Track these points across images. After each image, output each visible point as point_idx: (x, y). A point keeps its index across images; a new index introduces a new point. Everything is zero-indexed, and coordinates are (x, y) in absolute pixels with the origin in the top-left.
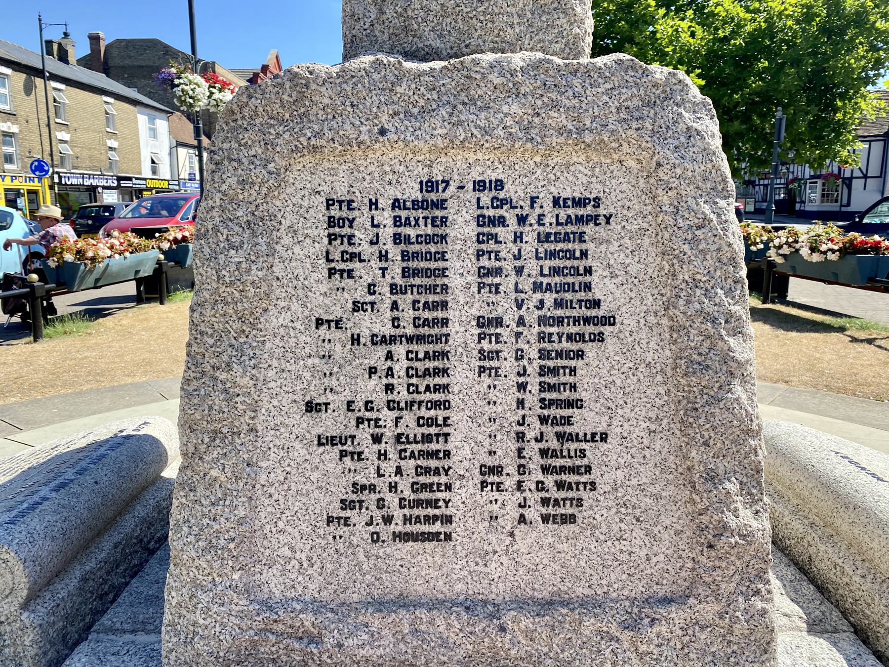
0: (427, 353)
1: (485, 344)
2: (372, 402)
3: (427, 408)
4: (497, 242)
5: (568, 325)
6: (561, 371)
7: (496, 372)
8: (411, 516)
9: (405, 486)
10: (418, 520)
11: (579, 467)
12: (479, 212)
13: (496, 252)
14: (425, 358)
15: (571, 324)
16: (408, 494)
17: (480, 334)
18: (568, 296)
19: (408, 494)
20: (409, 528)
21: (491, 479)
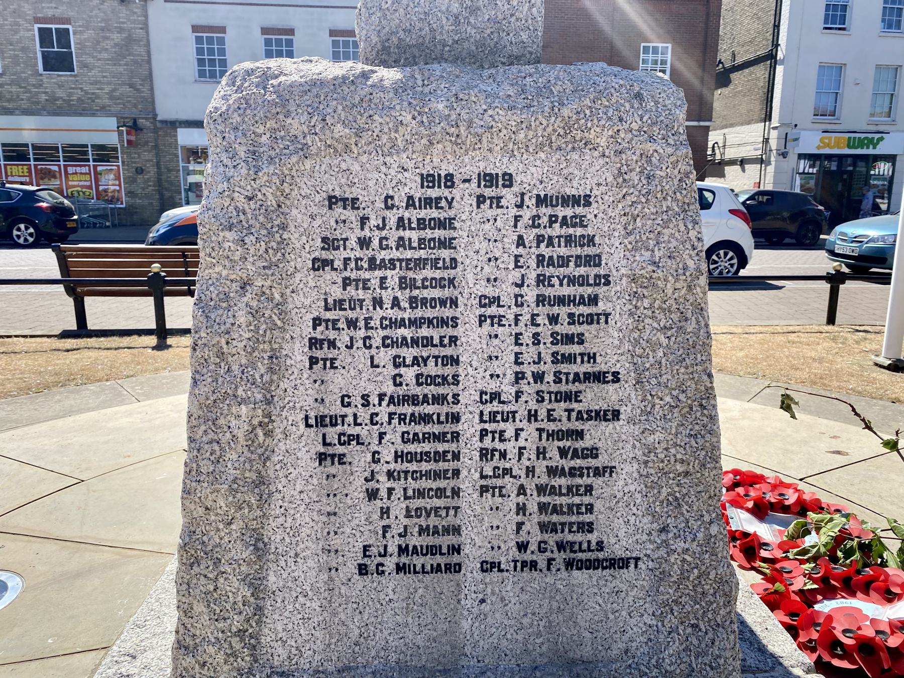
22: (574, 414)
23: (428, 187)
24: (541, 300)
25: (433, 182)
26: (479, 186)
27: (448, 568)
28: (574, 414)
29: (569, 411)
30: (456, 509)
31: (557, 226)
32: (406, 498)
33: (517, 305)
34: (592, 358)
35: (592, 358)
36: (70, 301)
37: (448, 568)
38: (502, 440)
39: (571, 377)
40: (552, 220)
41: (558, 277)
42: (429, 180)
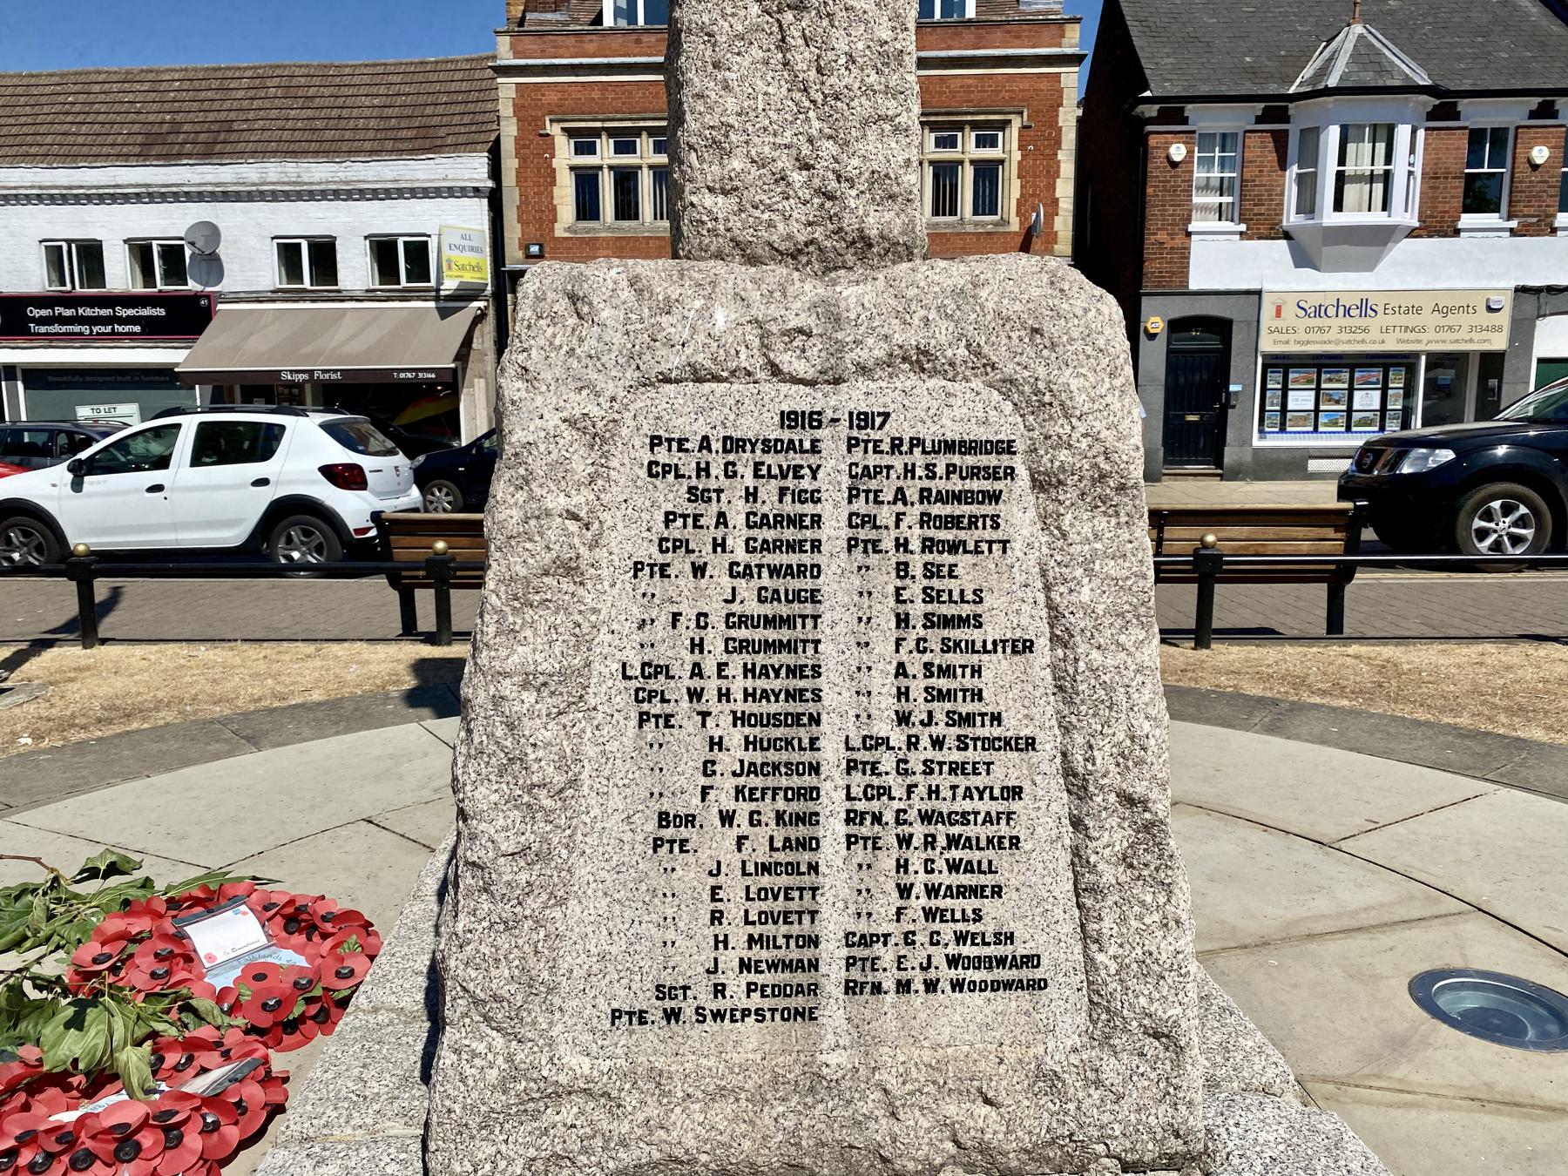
0: (787, 840)
1: (860, 506)
2: (706, 615)
3: (786, 799)
4: (875, 527)
5: (983, 725)
6: (978, 719)
7: (876, 496)
8: (754, 665)
9: (736, 543)
10: (765, 695)
11: (983, 887)
12: (848, 805)
13: (876, 441)
14: (784, 848)
15: (987, 722)
16: (741, 556)
17: (848, 959)
18: (970, 831)
19: (741, 556)
20: (751, 707)
21: (863, 534)
22: (960, 791)
23: (789, 427)
24: (930, 621)
25: (796, 420)
26: (851, 427)
27: (799, 1013)
28: (960, 791)
29: (954, 788)
30: (814, 890)
31: (955, 477)
32: (747, 922)
33: (927, 872)
34: (997, 718)
35: (997, 718)
36: (394, 596)
37: (799, 1013)
38: (877, 502)
39: (987, 795)
40: (951, 469)
41: (810, 467)
42: (790, 419)
